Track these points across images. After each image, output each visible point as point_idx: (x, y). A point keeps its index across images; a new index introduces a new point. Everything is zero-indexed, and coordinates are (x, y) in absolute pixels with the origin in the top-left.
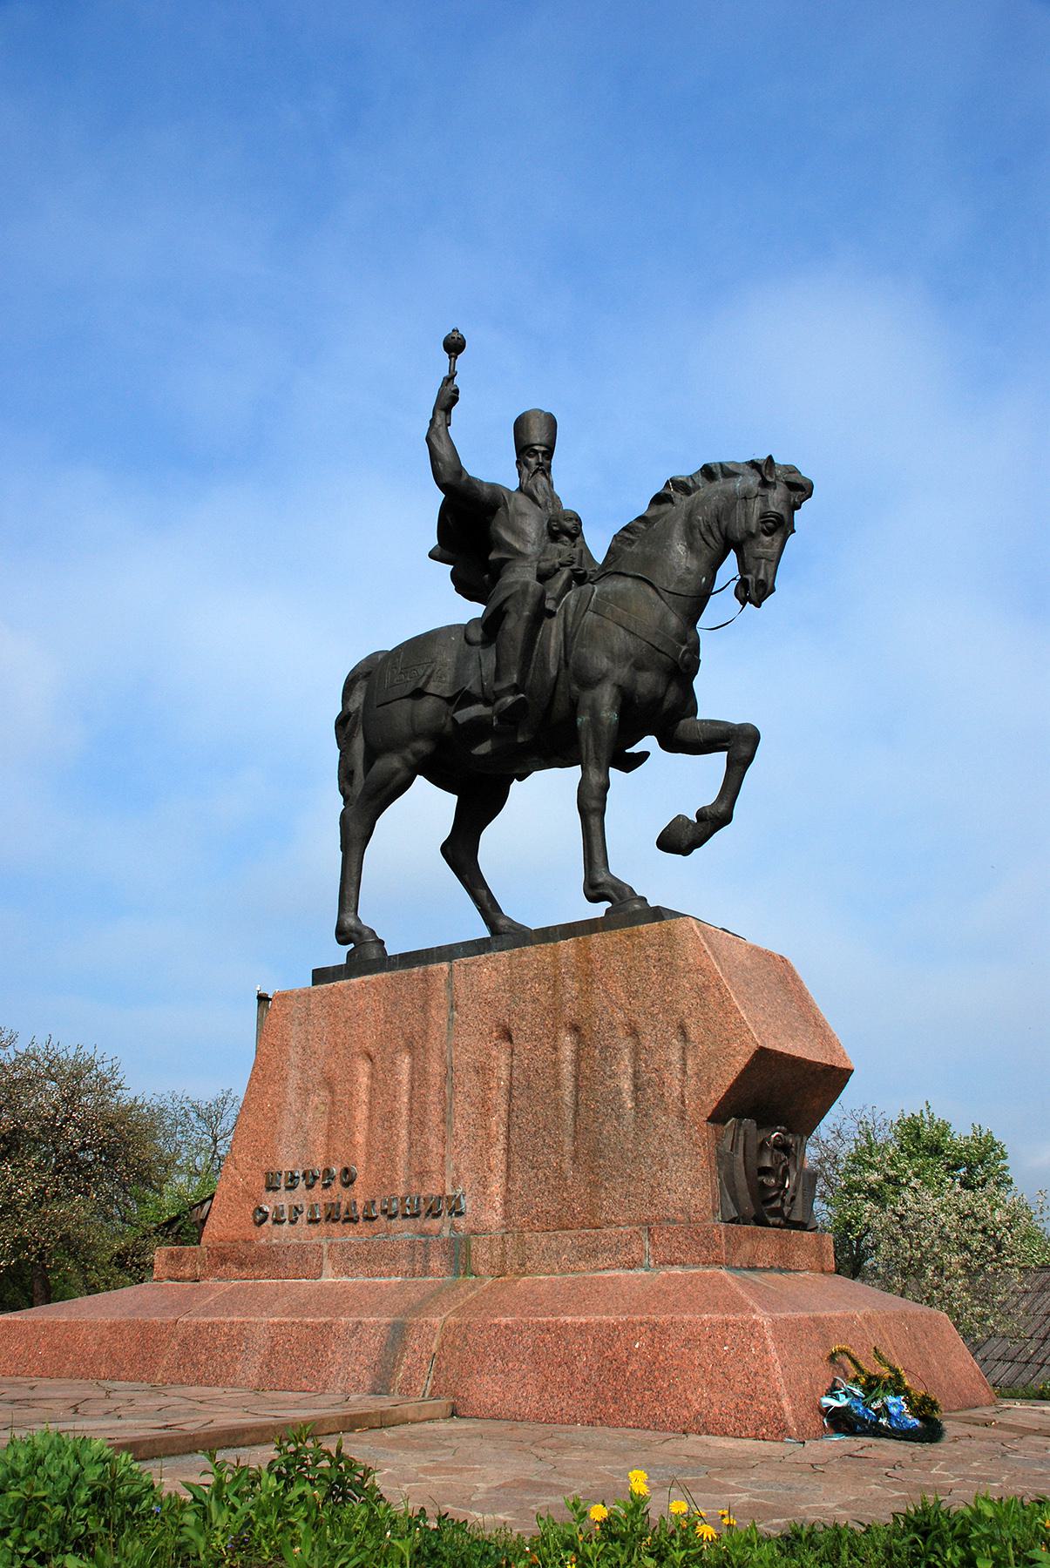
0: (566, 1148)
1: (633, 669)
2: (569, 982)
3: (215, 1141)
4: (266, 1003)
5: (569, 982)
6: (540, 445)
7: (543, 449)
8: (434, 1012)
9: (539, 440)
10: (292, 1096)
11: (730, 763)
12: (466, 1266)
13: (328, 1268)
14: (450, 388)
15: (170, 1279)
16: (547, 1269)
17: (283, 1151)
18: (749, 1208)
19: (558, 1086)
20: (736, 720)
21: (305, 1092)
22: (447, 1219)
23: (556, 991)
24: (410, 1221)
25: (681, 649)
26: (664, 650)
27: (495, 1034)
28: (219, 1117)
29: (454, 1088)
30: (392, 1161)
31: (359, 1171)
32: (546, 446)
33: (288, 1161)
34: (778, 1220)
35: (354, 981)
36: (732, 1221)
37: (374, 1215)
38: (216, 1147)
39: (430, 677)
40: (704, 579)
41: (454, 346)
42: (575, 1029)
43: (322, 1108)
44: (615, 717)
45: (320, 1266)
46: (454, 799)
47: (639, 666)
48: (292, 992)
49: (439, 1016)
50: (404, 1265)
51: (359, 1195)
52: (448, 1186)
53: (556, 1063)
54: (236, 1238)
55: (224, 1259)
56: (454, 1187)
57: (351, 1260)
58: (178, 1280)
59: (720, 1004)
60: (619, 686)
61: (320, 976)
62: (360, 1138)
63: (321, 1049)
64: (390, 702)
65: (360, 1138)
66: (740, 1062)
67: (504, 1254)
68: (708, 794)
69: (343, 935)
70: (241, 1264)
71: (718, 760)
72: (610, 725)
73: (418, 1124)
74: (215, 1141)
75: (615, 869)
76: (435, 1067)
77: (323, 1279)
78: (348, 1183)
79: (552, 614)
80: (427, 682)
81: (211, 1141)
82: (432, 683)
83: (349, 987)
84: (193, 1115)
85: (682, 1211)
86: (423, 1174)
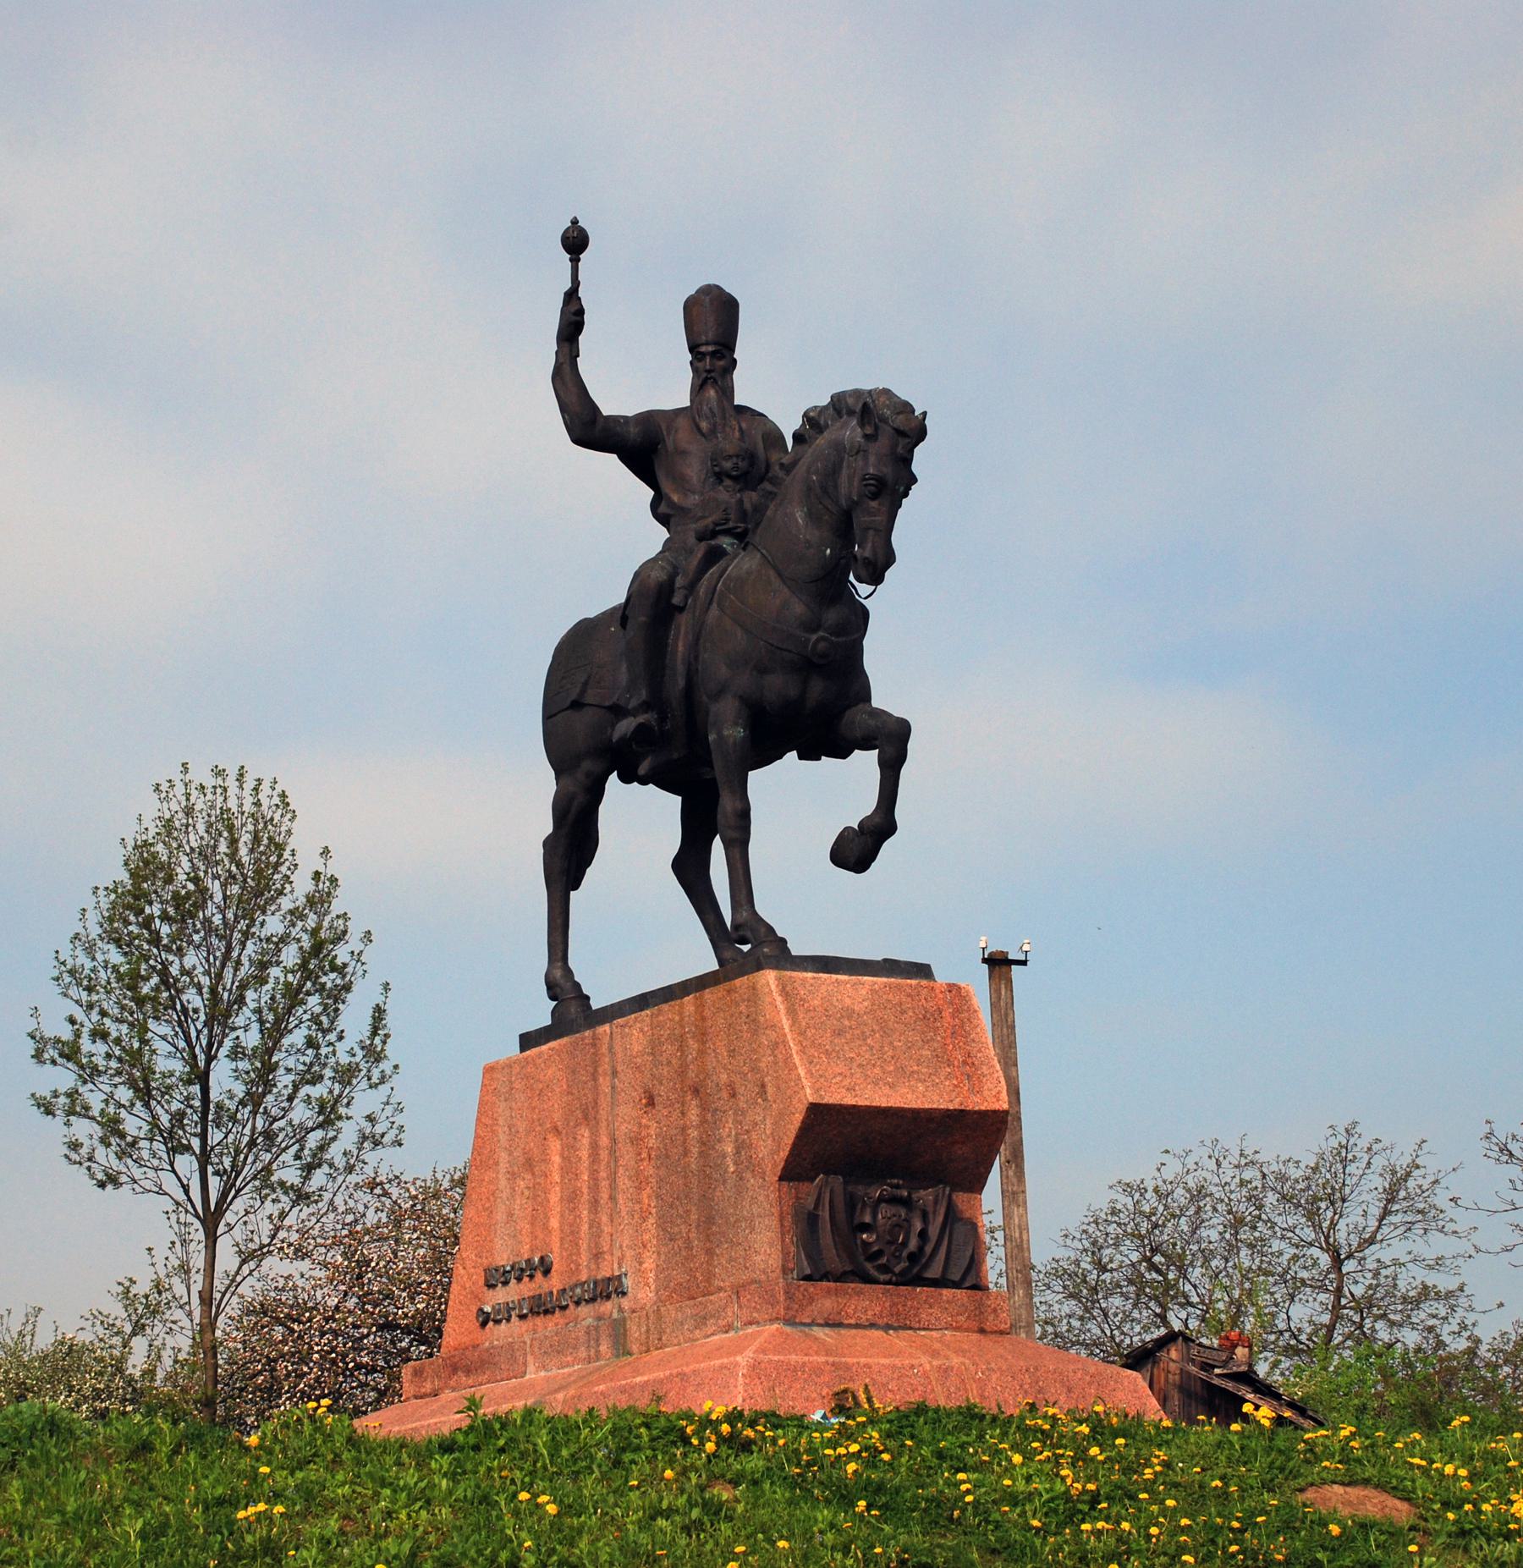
0: (693, 1217)
1: (755, 673)
2: (691, 1042)
3: (1337, 1262)
4: (1004, 969)
5: (691, 1042)
6: (707, 344)
7: (710, 348)
8: (601, 1079)
9: (704, 338)
10: (503, 1183)
11: (882, 763)
12: (624, 1346)
13: (531, 1368)
14: (573, 308)
15: (416, 1397)
16: (676, 1342)
17: (498, 1243)
18: (833, 1258)
19: (686, 1153)
20: (897, 713)
21: (513, 1176)
22: (616, 1300)
23: (683, 1052)
24: (590, 1306)
25: (808, 640)
26: (784, 647)
27: (644, 1101)
28: (1337, 1198)
29: (616, 1161)
30: (577, 1245)
31: (555, 1258)
32: (715, 344)
33: (503, 1259)
34: (886, 1277)
35: (544, 1047)
36: (807, 1278)
37: (564, 1303)
38: (1341, 1276)
39: (586, 684)
40: (828, 551)
41: (575, 242)
42: (696, 1091)
43: (527, 1193)
44: (740, 732)
45: (525, 1364)
46: (675, 802)
47: (762, 670)
48: (497, 1063)
49: (604, 1083)
50: (582, 1353)
51: (555, 1283)
52: (616, 1266)
53: (684, 1129)
54: (143, 1287)
55: (455, 1369)
56: (620, 1267)
57: (557, 1349)
58: (421, 1398)
59: (786, 1061)
60: (741, 697)
61: (528, 1041)
62: (554, 1223)
63: (522, 1126)
64: (555, 715)
65: (554, 1223)
66: (798, 1118)
67: (648, 1331)
68: (866, 804)
69: (553, 990)
70: (468, 1372)
71: (865, 763)
72: (735, 743)
73: (595, 1204)
74: (1337, 1262)
75: (761, 908)
76: (604, 1141)
77: (527, 1377)
78: (547, 1272)
79: (681, 609)
80: (583, 692)
81: (1325, 1260)
82: (589, 691)
83: (540, 1055)
84: (1271, 1198)
85: (764, 1272)
86: (597, 1256)
